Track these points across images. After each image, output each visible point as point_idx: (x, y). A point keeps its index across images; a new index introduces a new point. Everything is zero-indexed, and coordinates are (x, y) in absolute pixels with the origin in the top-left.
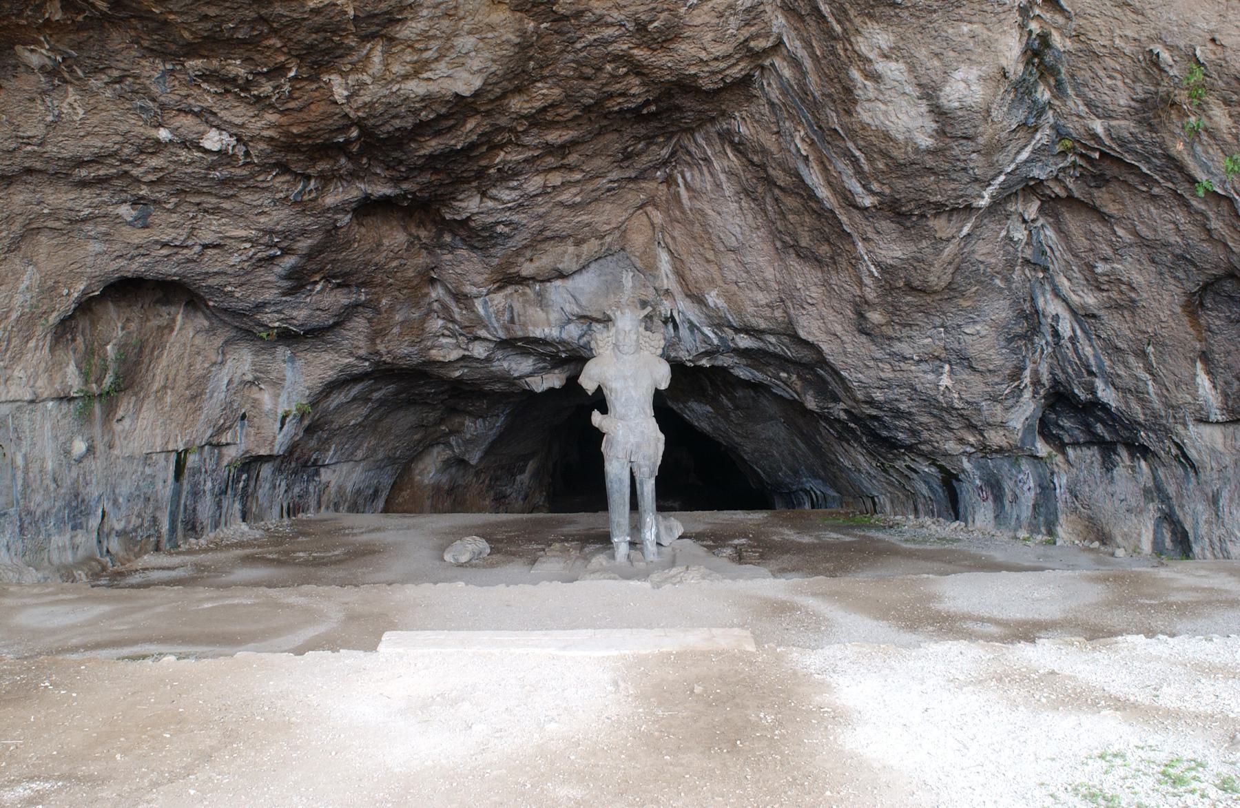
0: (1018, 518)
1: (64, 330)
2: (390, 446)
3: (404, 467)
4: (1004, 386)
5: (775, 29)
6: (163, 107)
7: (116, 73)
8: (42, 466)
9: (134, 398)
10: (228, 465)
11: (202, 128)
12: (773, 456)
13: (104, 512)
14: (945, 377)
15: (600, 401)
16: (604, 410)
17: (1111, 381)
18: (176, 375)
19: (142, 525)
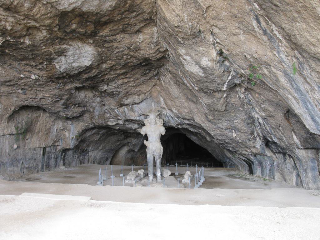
0: (266, 173)
1: (11, 118)
2: (110, 146)
3: (116, 152)
4: (250, 136)
5: (164, 46)
6: (20, 70)
7: (9, 64)
8: (6, 151)
9: (31, 134)
10: (59, 151)
11: (30, 74)
12: (216, 152)
13: (22, 163)
14: (234, 133)
15: (146, 138)
16: (147, 140)
17: (275, 136)
18: (42, 128)
19: (33, 166)
